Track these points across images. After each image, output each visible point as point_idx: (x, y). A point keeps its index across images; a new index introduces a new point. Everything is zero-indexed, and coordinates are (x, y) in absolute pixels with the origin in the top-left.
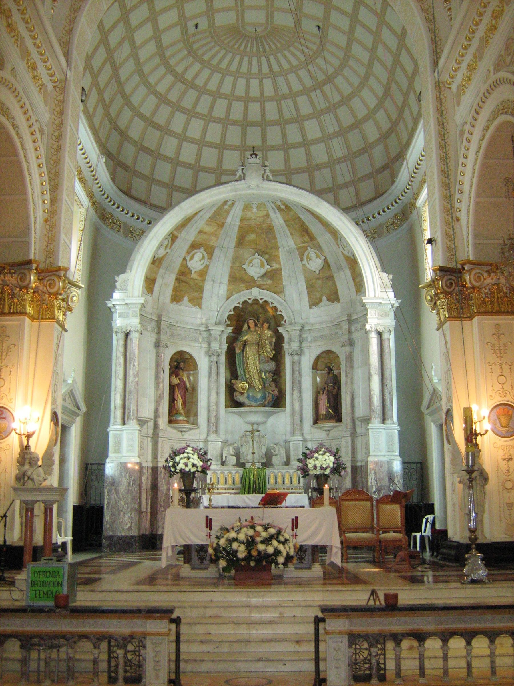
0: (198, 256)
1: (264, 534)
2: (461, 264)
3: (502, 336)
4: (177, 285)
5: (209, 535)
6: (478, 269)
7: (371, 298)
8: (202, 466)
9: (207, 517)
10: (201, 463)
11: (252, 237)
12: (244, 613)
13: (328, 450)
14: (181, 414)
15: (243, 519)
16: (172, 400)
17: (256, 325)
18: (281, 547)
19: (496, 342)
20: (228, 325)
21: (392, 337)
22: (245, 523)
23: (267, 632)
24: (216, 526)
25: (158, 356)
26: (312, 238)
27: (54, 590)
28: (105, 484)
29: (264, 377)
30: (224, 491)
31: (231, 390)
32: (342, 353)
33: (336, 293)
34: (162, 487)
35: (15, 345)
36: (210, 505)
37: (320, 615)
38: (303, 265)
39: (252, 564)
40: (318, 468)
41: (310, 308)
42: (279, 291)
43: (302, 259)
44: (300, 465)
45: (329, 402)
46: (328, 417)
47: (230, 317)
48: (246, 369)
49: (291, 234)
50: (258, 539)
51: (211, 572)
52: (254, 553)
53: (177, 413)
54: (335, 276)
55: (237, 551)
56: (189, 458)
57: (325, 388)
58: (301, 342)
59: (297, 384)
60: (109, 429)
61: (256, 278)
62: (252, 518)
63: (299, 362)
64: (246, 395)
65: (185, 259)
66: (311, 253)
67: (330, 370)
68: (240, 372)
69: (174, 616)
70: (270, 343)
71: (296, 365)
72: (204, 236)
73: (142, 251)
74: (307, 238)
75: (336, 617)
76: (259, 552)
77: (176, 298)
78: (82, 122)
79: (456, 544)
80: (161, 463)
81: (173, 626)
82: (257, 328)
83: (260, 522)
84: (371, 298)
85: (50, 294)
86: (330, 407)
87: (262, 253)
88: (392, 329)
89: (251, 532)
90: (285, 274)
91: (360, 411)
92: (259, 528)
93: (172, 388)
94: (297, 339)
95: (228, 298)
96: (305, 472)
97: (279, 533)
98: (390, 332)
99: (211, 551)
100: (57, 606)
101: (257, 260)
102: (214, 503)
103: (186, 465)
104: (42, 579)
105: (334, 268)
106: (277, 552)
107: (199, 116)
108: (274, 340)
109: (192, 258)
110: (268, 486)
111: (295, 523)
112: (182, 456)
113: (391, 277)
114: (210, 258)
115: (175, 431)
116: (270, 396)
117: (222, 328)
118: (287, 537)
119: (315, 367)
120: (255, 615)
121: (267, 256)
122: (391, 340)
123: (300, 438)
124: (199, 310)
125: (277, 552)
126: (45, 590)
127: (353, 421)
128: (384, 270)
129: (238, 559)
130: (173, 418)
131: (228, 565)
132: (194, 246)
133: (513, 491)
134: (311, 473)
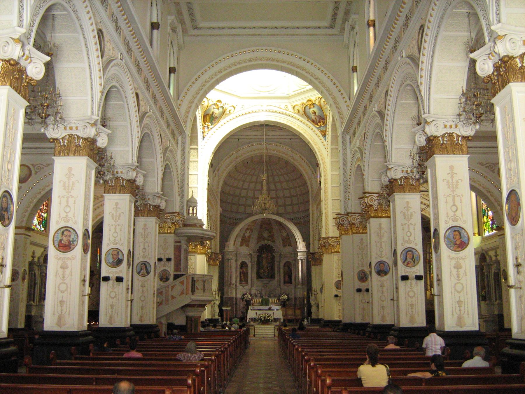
0: (248, 232)
16: (240, 276)
19: (406, 212)
20: (257, 252)
21: (306, 261)
25: (236, 264)
33: (291, 243)
34: (238, 303)
42: (274, 241)
46: (288, 283)
47: (258, 249)
51: (257, 323)
58: (280, 258)
71: (279, 265)
77: (241, 245)
78: (171, 96)
79: (442, 332)
88: (306, 259)
90: (275, 236)
96: (279, 300)
101: (266, 232)
102: (254, 309)
106: (270, 319)
111: (273, 314)
120: (265, 329)
122: (305, 262)
125: (270, 319)
127: (295, 284)
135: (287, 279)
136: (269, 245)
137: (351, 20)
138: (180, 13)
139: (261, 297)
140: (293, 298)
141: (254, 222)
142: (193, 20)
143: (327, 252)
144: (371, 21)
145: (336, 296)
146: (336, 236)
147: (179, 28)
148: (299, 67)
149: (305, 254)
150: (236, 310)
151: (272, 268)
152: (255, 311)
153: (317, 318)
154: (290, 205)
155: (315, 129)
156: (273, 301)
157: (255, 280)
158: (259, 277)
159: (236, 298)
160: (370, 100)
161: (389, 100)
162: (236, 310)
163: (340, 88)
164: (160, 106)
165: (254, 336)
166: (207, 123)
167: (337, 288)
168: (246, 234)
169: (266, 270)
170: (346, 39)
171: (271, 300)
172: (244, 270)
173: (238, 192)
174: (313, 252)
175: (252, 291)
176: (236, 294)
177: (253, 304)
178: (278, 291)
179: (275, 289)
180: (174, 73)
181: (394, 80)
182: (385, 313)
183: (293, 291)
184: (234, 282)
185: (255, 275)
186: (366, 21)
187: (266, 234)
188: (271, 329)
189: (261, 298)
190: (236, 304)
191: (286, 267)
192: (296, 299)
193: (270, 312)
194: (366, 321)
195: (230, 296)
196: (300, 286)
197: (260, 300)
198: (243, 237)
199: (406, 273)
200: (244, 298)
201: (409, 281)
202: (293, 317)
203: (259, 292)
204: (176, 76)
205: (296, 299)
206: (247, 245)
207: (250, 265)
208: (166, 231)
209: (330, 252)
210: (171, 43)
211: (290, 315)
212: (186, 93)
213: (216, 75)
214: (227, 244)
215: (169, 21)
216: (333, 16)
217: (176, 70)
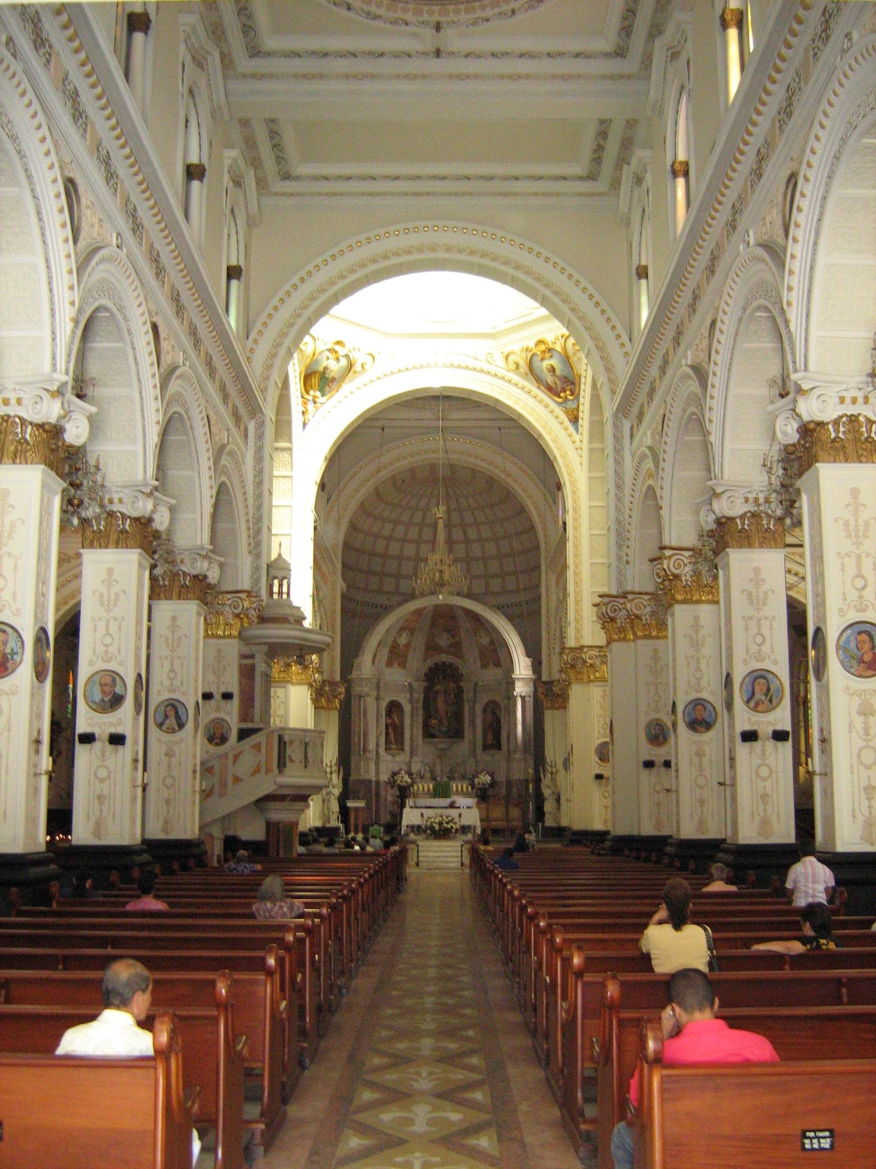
0: (404, 635)
3: (861, 508)
16: (387, 734)
20: (424, 681)
21: (532, 700)
24: (425, 817)
25: (378, 707)
31: (426, 725)
32: (503, 703)
33: (499, 660)
34: (383, 794)
42: (461, 657)
47: (426, 675)
48: (437, 711)
54: (498, 650)
58: (475, 693)
59: (473, 722)
66: (483, 633)
67: (494, 713)
77: (389, 664)
78: (233, 333)
80: (384, 777)
87: (448, 631)
88: (532, 695)
91: (512, 747)
96: (473, 785)
101: (445, 636)
106: (452, 827)
111: (460, 815)
119: (484, 710)
122: (530, 701)
123: (473, 760)
125: (452, 827)
127: (509, 751)
137: (634, 161)
138: (250, 143)
139: (434, 779)
141: (418, 613)
142: (280, 159)
144: (681, 163)
145: (599, 777)
147: (214, 60)
148: (517, 267)
149: (531, 685)
150: (377, 809)
151: (458, 716)
152: (419, 811)
155: (553, 406)
157: (420, 739)
158: (428, 734)
159: (378, 782)
160: (677, 342)
161: (719, 342)
162: (377, 809)
163: (610, 313)
164: (207, 354)
165: (417, 864)
166: (312, 392)
167: (600, 759)
170: (623, 206)
171: (454, 786)
172: (396, 719)
173: (381, 545)
177: (415, 796)
178: (471, 765)
179: (465, 762)
180: (238, 277)
181: (730, 296)
183: (503, 763)
184: (372, 746)
185: (419, 732)
186: (669, 163)
187: (443, 641)
188: (454, 849)
189: (434, 782)
190: (378, 794)
191: (489, 714)
192: (509, 783)
193: (454, 813)
194: (665, 832)
195: (364, 776)
197: (431, 787)
200: (395, 781)
203: (427, 769)
204: (205, 191)
205: (509, 783)
206: (403, 665)
207: (407, 708)
208: (220, 633)
210: (232, 211)
212: (265, 325)
213: (333, 284)
214: (356, 662)
215: (227, 163)
216: (595, 151)
217: (243, 272)
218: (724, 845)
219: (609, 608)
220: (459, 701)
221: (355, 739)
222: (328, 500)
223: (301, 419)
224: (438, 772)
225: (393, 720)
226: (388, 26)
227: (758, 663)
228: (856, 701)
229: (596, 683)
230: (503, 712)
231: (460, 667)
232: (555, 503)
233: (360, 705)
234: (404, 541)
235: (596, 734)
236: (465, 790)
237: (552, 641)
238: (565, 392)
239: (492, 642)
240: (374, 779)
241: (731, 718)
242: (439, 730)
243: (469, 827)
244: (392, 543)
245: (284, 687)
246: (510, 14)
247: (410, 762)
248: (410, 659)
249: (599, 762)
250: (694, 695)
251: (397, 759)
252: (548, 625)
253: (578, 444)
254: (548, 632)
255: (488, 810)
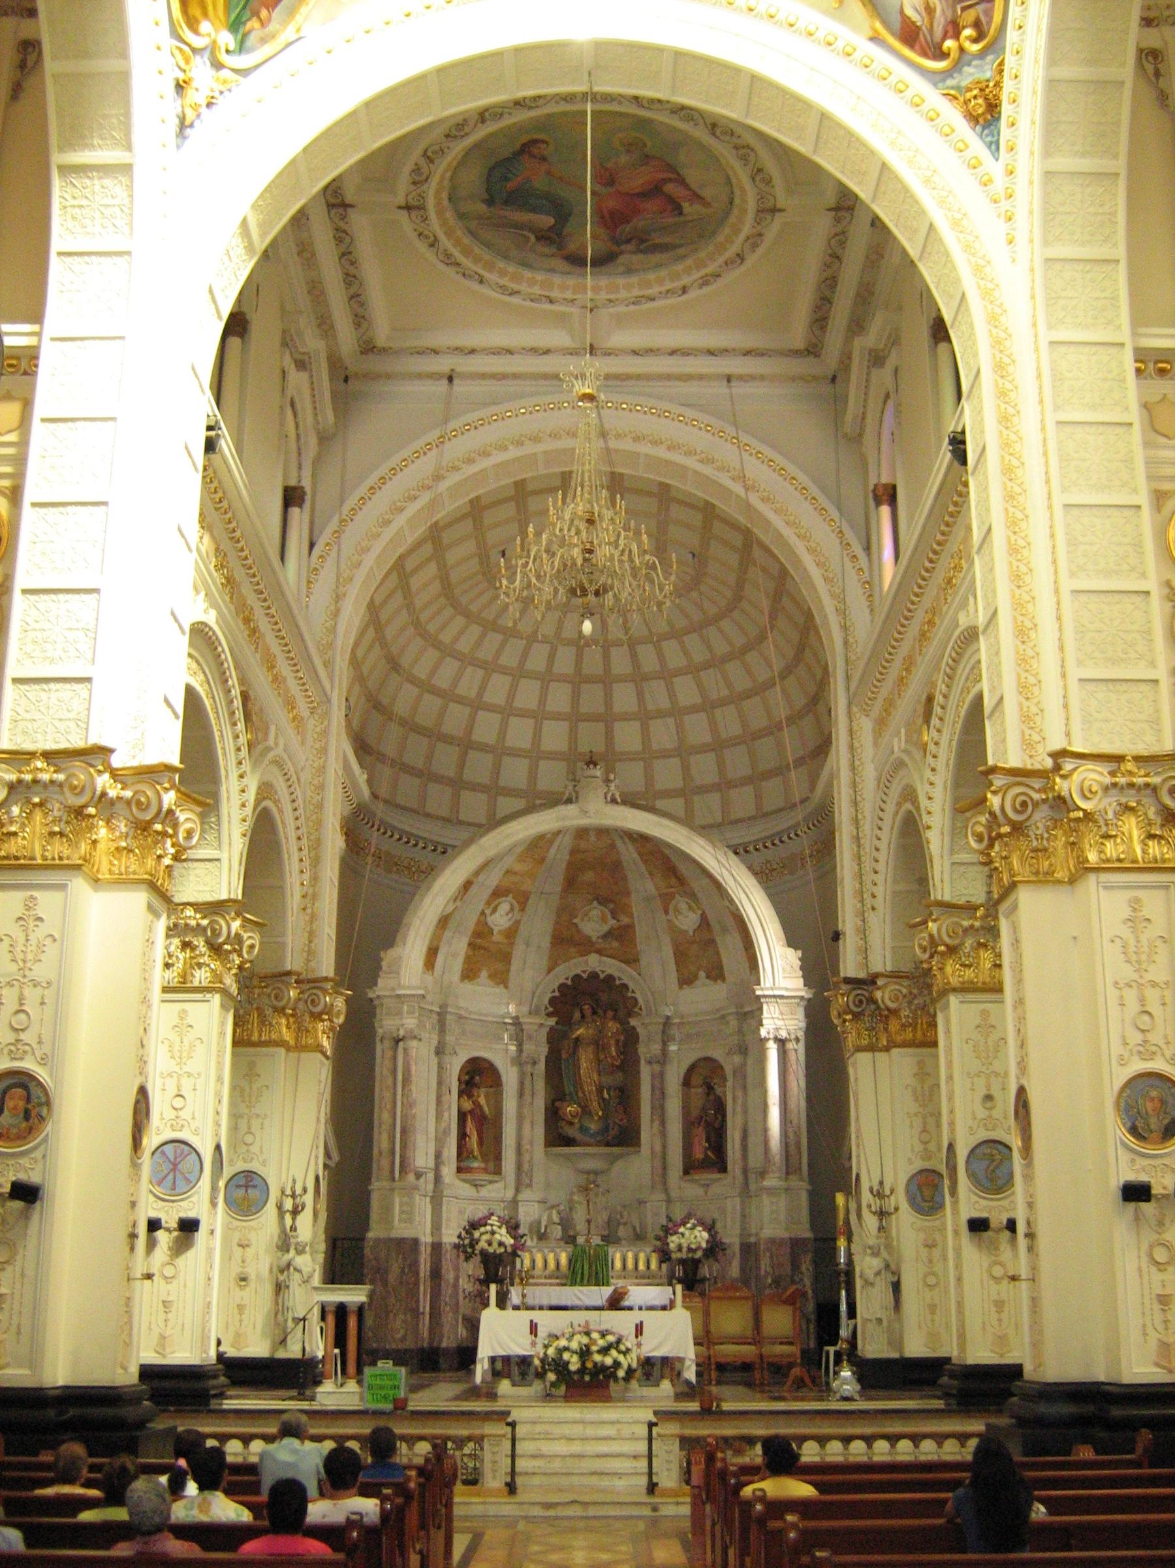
0: (504, 907)
1: (601, 1343)
2: (1051, 755)
4: (471, 953)
5: (534, 1344)
6: (896, 983)
7: (767, 989)
8: (512, 1246)
9: (531, 1321)
10: (512, 1241)
11: (589, 876)
12: (577, 1430)
13: (701, 1223)
14: (475, 1158)
15: (575, 1324)
16: (462, 1136)
17: (594, 1013)
18: (621, 1358)
20: (549, 1015)
21: (801, 1047)
22: (578, 1329)
23: (604, 1448)
24: (542, 1332)
25: (440, 1067)
26: (682, 881)
27: (391, 1393)
28: (365, 1271)
29: (606, 1096)
30: (543, 1281)
31: (553, 1115)
32: (729, 1064)
34: (449, 1275)
35: (267, 1087)
36: (523, 1303)
37: (654, 1420)
38: (669, 921)
39: (587, 1378)
40: (685, 1250)
41: (681, 987)
42: (632, 960)
43: (666, 912)
44: (658, 1243)
45: (708, 1140)
47: (553, 1001)
48: (577, 1082)
49: (651, 874)
50: (594, 1348)
51: (537, 1387)
52: (589, 1365)
53: (470, 1155)
54: (718, 939)
55: (568, 1363)
56: (493, 1233)
57: (702, 1117)
59: (660, 1111)
60: (371, 1187)
61: (594, 939)
62: (587, 1323)
63: (662, 1075)
64: (577, 1126)
65: (483, 913)
66: (682, 903)
68: (568, 1088)
69: (510, 1420)
70: (617, 1041)
71: (659, 1080)
72: (516, 879)
73: (421, 913)
74: (673, 881)
75: (668, 1420)
76: (595, 1364)
77: (469, 974)
80: (450, 1236)
81: (509, 1429)
82: (595, 1017)
83: (598, 1328)
84: (767, 989)
85: (312, 1014)
86: (710, 1147)
87: (603, 901)
88: (801, 1034)
89: (585, 1340)
90: (641, 931)
91: (755, 1161)
92: (595, 1335)
93: (462, 1116)
94: (659, 1038)
95: (549, 971)
96: (665, 1255)
97: (619, 1341)
98: (797, 1040)
99: (537, 1362)
100: (396, 1408)
101: (596, 911)
102: (530, 1301)
103: (490, 1244)
104: (378, 1382)
105: (716, 927)
106: (617, 1364)
107: (504, 670)
108: (622, 1038)
109: (494, 911)
110: (611, 1274)
111: (639, 1329)
112: (482, 1229)
113: (799, 953)
114: (522, 910)
115: (467, 1185)
116: (616, 1128)
117: (538, 1020)
118: (629, 1346)
119: (686, 1083)
120: (590, 1431)
121: (612, 906)
122: (798, 1052)
123: (663, 1196)
124: (504, 990)
125: (617, 1364)
126: (383, 1393)
127: (745, 1171)
128: (790, 944)
129: (569, 1372)
130: (464, 1164)
131: (558, 1379)
132: (498, 893)
133: (1171, 1269)
134: (674, 1256)
135: (700, 1150)
136: (610, 978)
139: (569, 1239)
140: (737, 1248)
141: (538, 845)
143: (1044, 879)
145: (1135, 1193)
146: (1106, 748)
149: (800, 1013)
150: (435, 1313)
151: (626, 1096)
152: (526, 1316)
153: (895, 1355)
154: (716, 787)
155: (920, 85)
156: (630, 1264)
157: (537, 1149)
158: (557, 1137)
159: (437, 1247)
162: (435, 1313)
165: (511, 1488)
166: (205, 26)
167: (1134, 1131)
168: (490, 920)
169: (595, 1105)
171: (618, 1256)
172: (482, 1101)
173: (455, 719)
174: (862, 975)
175: (521, 1210)
176: (437, 1227)
177: (526, 1279)
178: (654, 1215)
179: (641, 1202)
182: (244, 1323)
183: (733, 1205)
184: (423, 1158)
185: (539, 1132)
187: (593, 924)
188: (626, 1431)
189: (570, 1248)
190: (436, 1274)
191: (698, 1091)
192: (748, 1250)
193: (620, 1322)
194: (941, 1353)
195: (401, 1230)
196: (771, 1181)
197: (564, 1259)
198: (477, 934)
199: (981, 1210)
200: (473, 1243)
201: (990, 1233)
202: (747, 1351)
203: (556, 1218)
205: (748, 1250)
206: (501, 978)
207: (510, 1077)
208: (255, 1037)
209: (1062, 868)
211: (775, 1341)
214: (388, 957)
216: (818, 308)
218: (948, 1367)
219: (851, 998)
220: (628, 1062)
221: (381, 1141)
222: (312, 545)
223: (172, 106)
224: (581, 1226)
225: (477, 1104)
226: (528, 303)
227: (989, 1133)
228: (922, 1236)
229: (1104, 877)
230: (729, 1084)
231: (631, 986)
232: (868, 548)
233: (395, 1058)
234: (508, 711)
235: (1116, 1049)
236: (642, 1266)
237: (868, 878)
238: (957, 36)
239: (704, 922)
240: (426, 1238)
241: (955, 1203)
242: (583, 1129)
243: (665, 1361)
244: (482, 715)
245: (62, 887)
246: (680, 292)
247: (515, 1203)
248: (515, 965)
249: (1130, 1140)
250: (983, 1135)
251: (486, 1192)
252: (857, 839)
253: (1000, 183)
254: (858, 858)
255: (707, 1314)
